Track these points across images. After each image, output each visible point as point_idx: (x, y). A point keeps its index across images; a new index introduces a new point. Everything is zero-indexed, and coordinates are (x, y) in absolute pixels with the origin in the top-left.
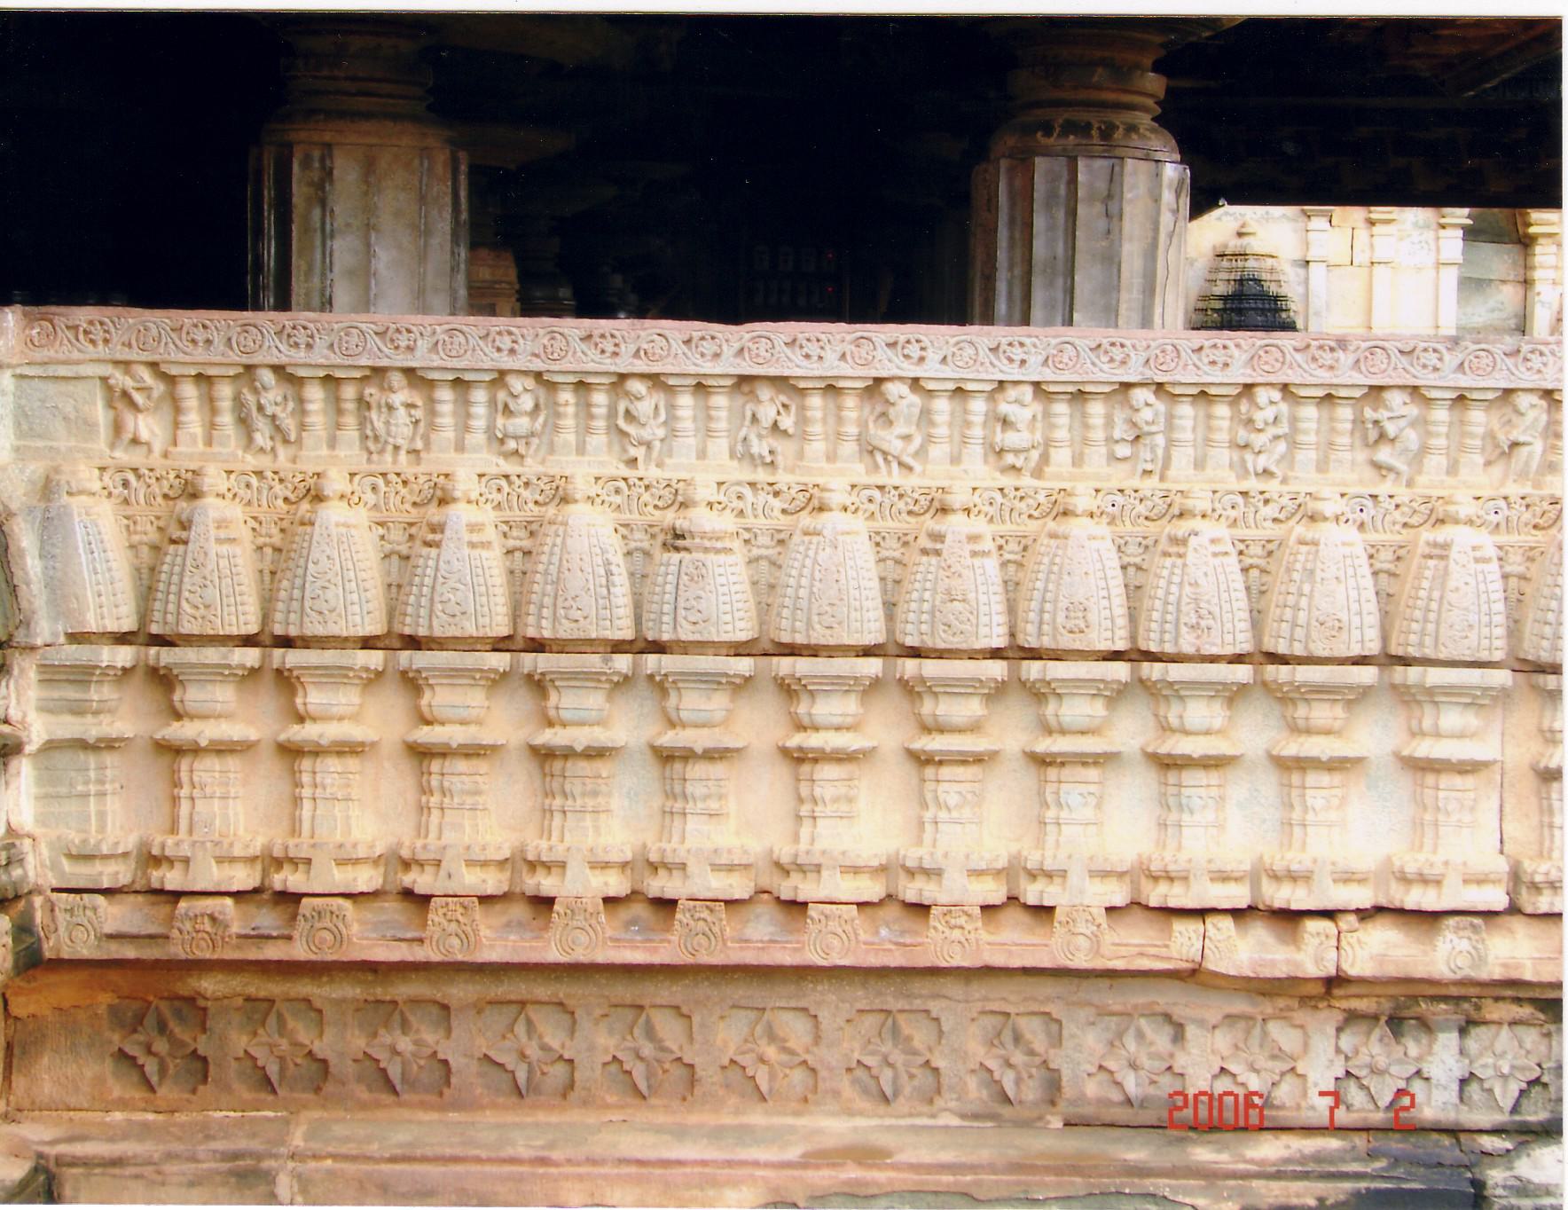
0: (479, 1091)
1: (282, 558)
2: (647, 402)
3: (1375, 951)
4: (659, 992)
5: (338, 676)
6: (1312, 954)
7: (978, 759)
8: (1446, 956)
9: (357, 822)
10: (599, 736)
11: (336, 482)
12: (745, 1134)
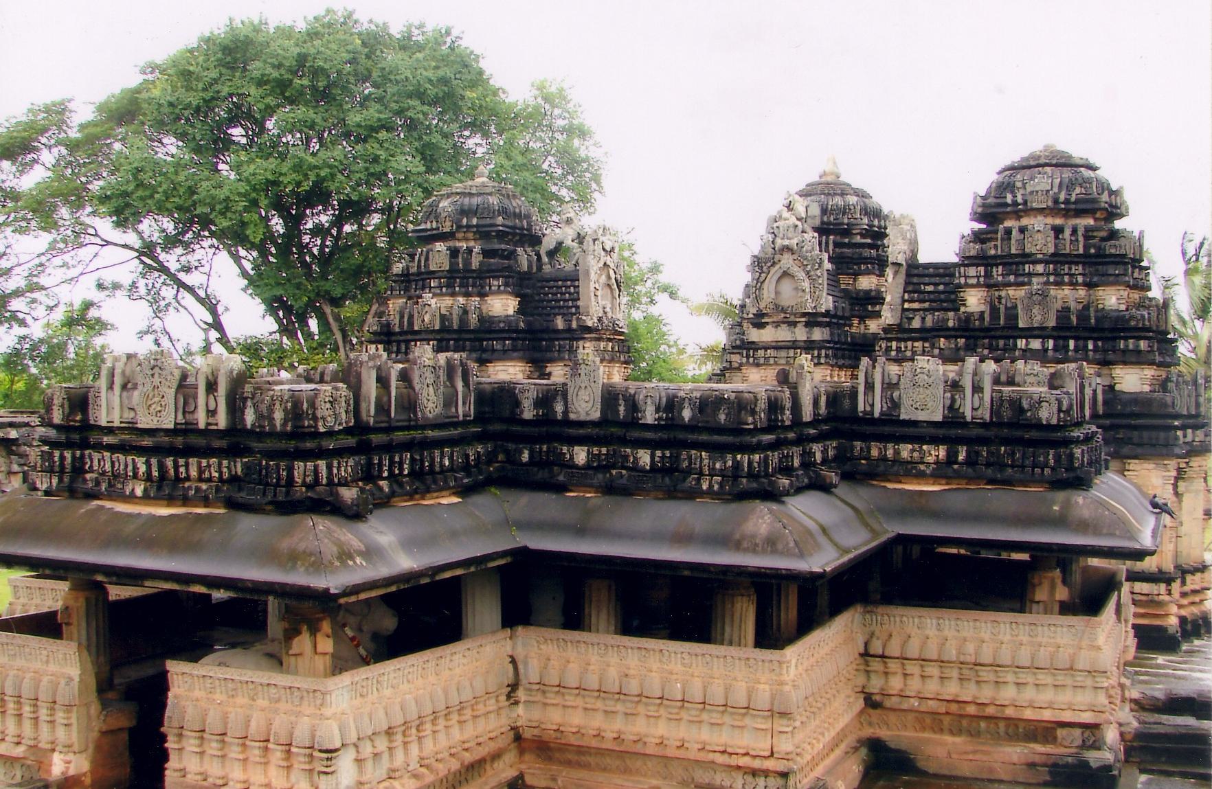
0: (387, 692)
1: (924, 644)
2: (623, 650)
3: (743, 761)
4: (625, 756)
5: (570, 694)
6: (734, 761)
7: (742, 727)
8: (757, 764)
9: (575, 719)
10: (614, 709)
11: (572, 659)
12: (639, 782)
